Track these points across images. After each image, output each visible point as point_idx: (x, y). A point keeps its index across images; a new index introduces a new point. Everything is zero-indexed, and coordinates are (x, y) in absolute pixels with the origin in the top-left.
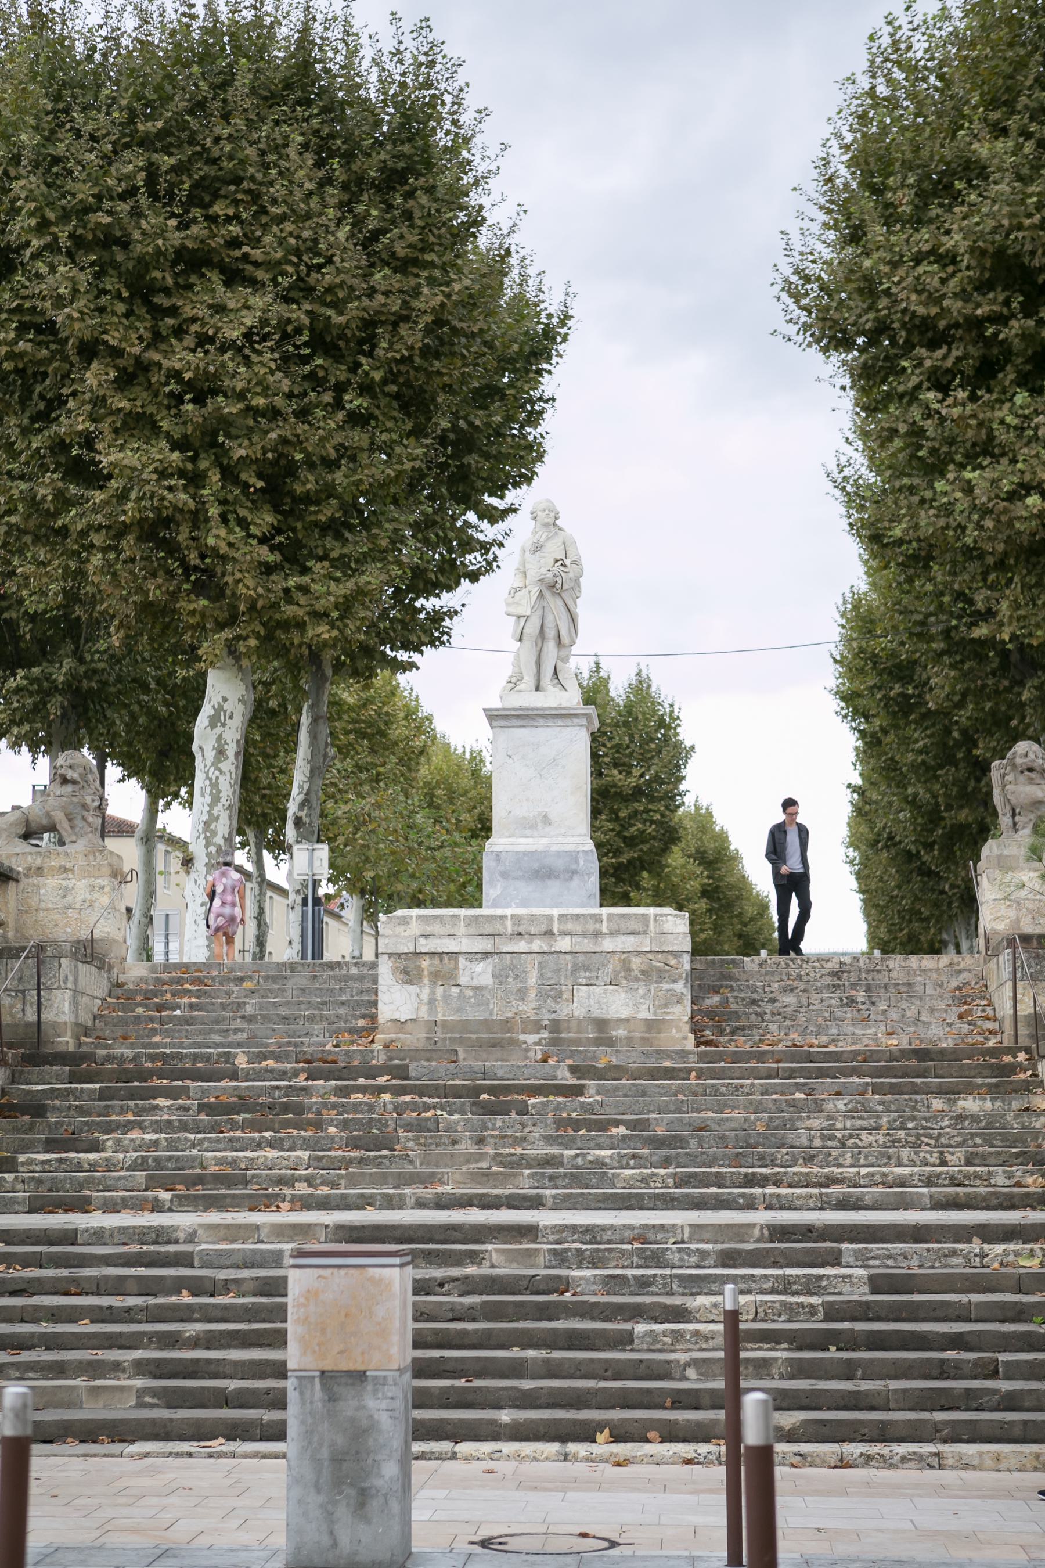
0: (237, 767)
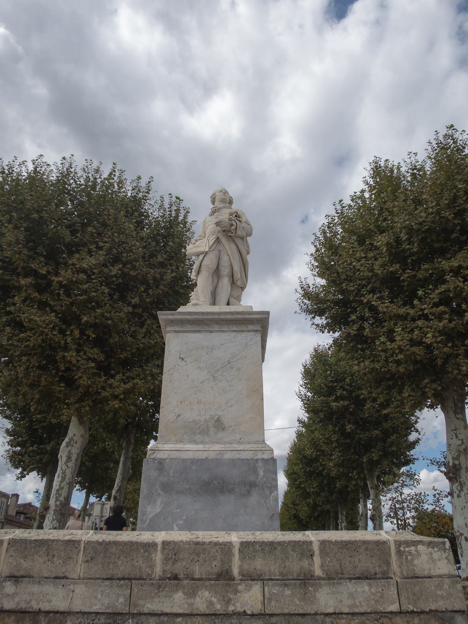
0: (76, 465)
